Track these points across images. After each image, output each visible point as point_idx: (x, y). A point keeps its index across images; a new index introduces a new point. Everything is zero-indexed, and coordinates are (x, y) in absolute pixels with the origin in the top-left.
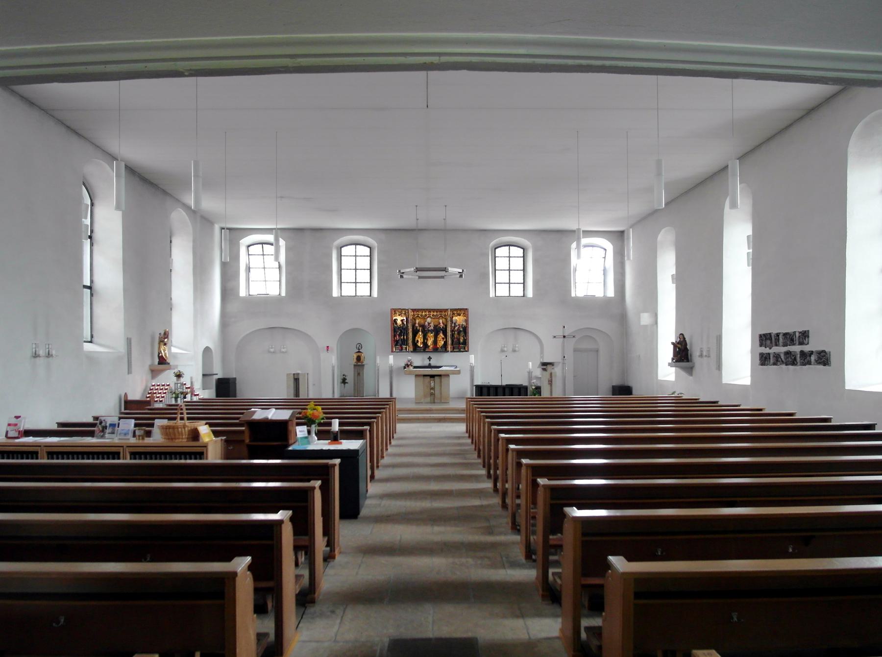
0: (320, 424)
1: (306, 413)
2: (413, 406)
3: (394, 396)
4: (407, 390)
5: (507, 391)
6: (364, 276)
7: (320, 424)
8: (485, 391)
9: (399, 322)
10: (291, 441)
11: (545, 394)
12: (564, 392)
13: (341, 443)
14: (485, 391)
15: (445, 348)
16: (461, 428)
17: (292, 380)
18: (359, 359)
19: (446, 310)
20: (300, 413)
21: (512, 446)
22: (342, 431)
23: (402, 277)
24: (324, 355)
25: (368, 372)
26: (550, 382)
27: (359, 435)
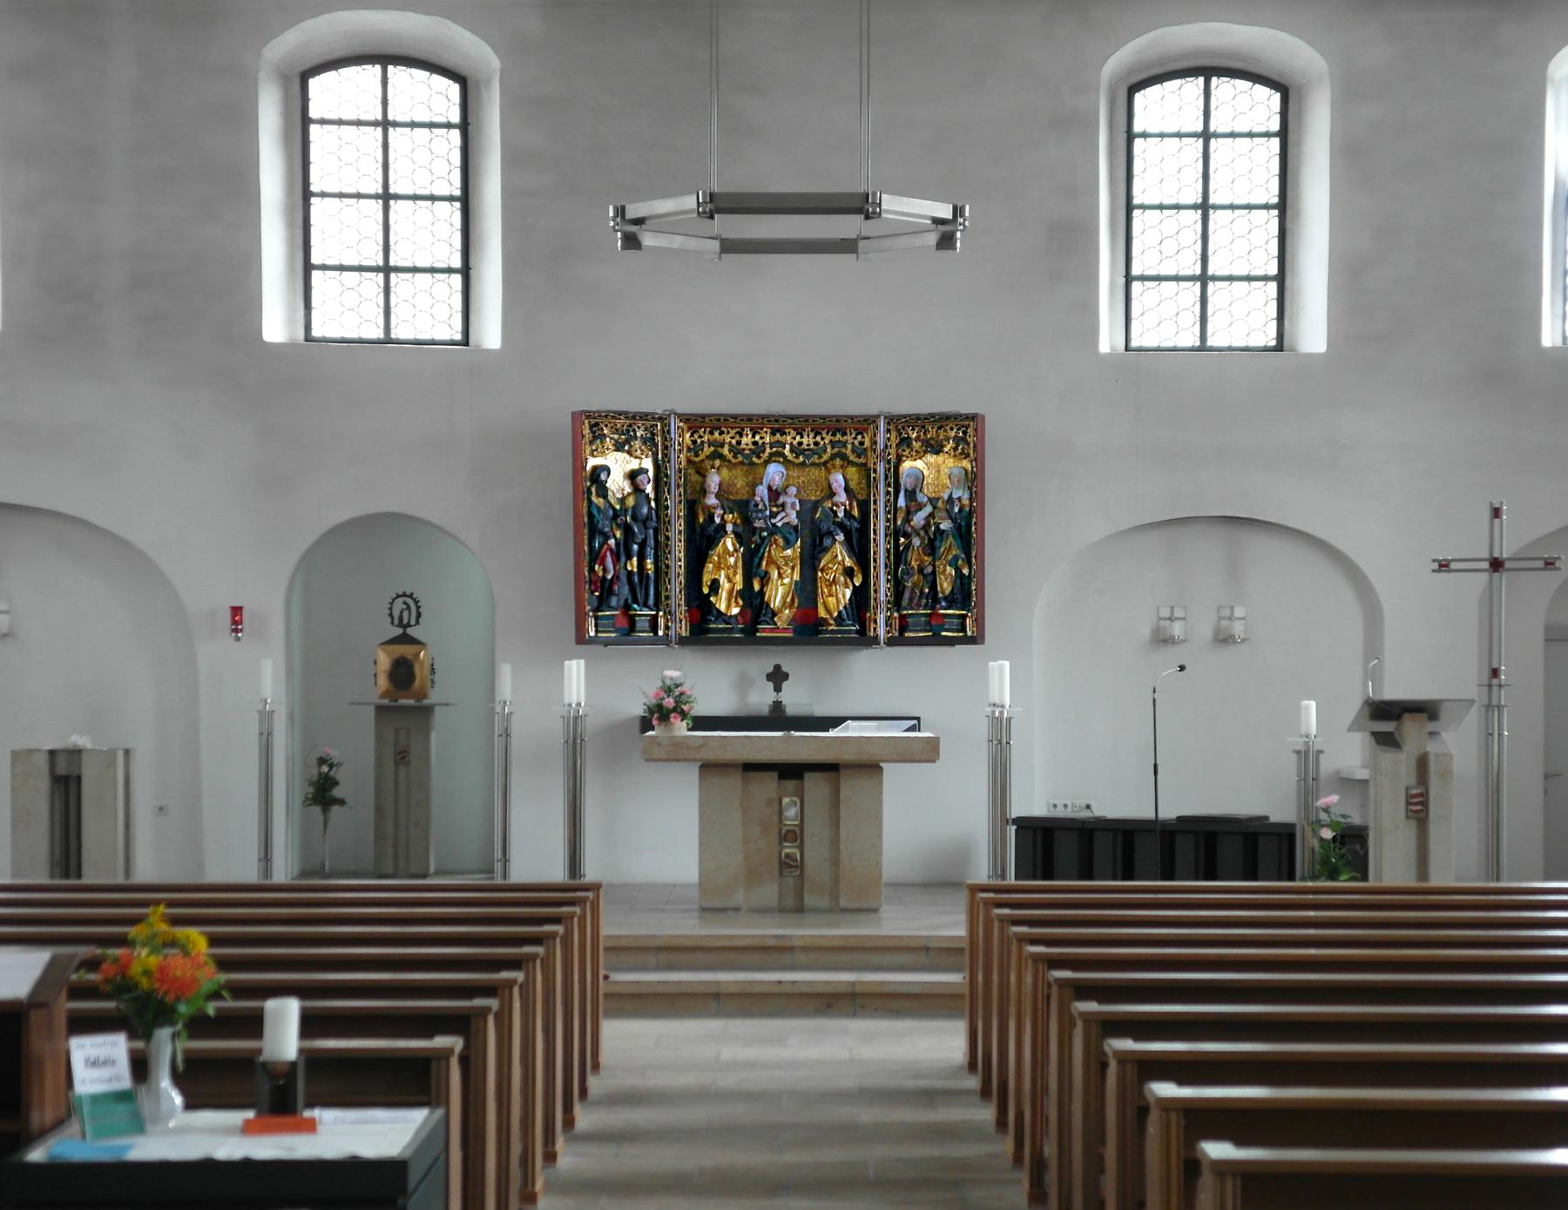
0: (199, 1026)
1: (123, 966)
2: (688, 927)
3: (591, 873)
4: (656, 841)
5: (1185, 851)
6: (430, 234)
7: (199, 1026)
8: (1185, 851)
9: (617, 483)
10: (40, 1116)
11: (1391, 865)
12: (1494, 866)
13: (310, 1126)
14: (1066, 849)
15: (856, 627)
16: (941, 1045)
17: (44, 784)
18: (402, 674)
19: (864, 423)
20: (92, 964)
21: (1217, 1150)
22: (313, 1061)
23: (632, 242)
24: (215, 650)
25: (450, 745)
26: (1419, 808)
27: (399, 1083)
